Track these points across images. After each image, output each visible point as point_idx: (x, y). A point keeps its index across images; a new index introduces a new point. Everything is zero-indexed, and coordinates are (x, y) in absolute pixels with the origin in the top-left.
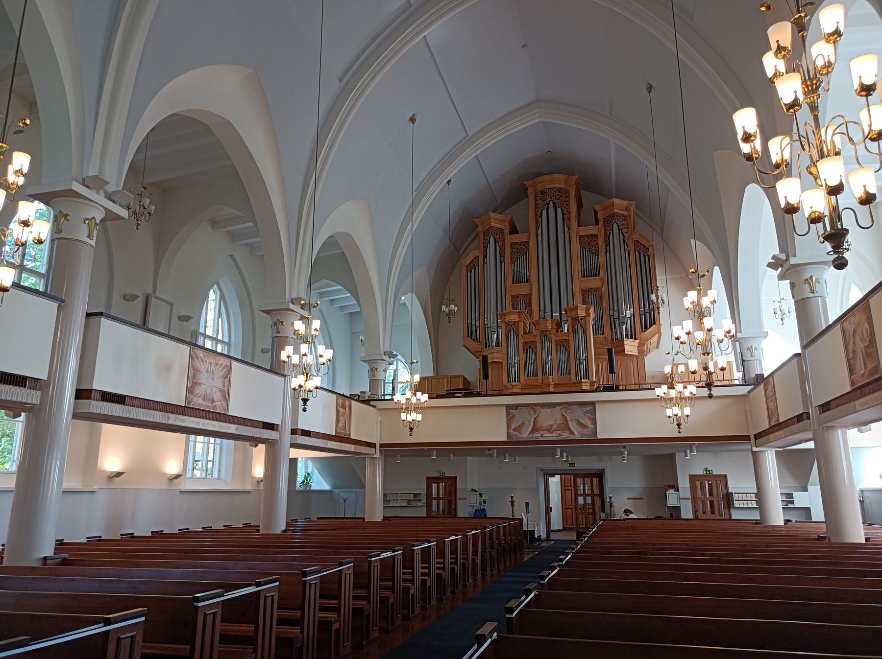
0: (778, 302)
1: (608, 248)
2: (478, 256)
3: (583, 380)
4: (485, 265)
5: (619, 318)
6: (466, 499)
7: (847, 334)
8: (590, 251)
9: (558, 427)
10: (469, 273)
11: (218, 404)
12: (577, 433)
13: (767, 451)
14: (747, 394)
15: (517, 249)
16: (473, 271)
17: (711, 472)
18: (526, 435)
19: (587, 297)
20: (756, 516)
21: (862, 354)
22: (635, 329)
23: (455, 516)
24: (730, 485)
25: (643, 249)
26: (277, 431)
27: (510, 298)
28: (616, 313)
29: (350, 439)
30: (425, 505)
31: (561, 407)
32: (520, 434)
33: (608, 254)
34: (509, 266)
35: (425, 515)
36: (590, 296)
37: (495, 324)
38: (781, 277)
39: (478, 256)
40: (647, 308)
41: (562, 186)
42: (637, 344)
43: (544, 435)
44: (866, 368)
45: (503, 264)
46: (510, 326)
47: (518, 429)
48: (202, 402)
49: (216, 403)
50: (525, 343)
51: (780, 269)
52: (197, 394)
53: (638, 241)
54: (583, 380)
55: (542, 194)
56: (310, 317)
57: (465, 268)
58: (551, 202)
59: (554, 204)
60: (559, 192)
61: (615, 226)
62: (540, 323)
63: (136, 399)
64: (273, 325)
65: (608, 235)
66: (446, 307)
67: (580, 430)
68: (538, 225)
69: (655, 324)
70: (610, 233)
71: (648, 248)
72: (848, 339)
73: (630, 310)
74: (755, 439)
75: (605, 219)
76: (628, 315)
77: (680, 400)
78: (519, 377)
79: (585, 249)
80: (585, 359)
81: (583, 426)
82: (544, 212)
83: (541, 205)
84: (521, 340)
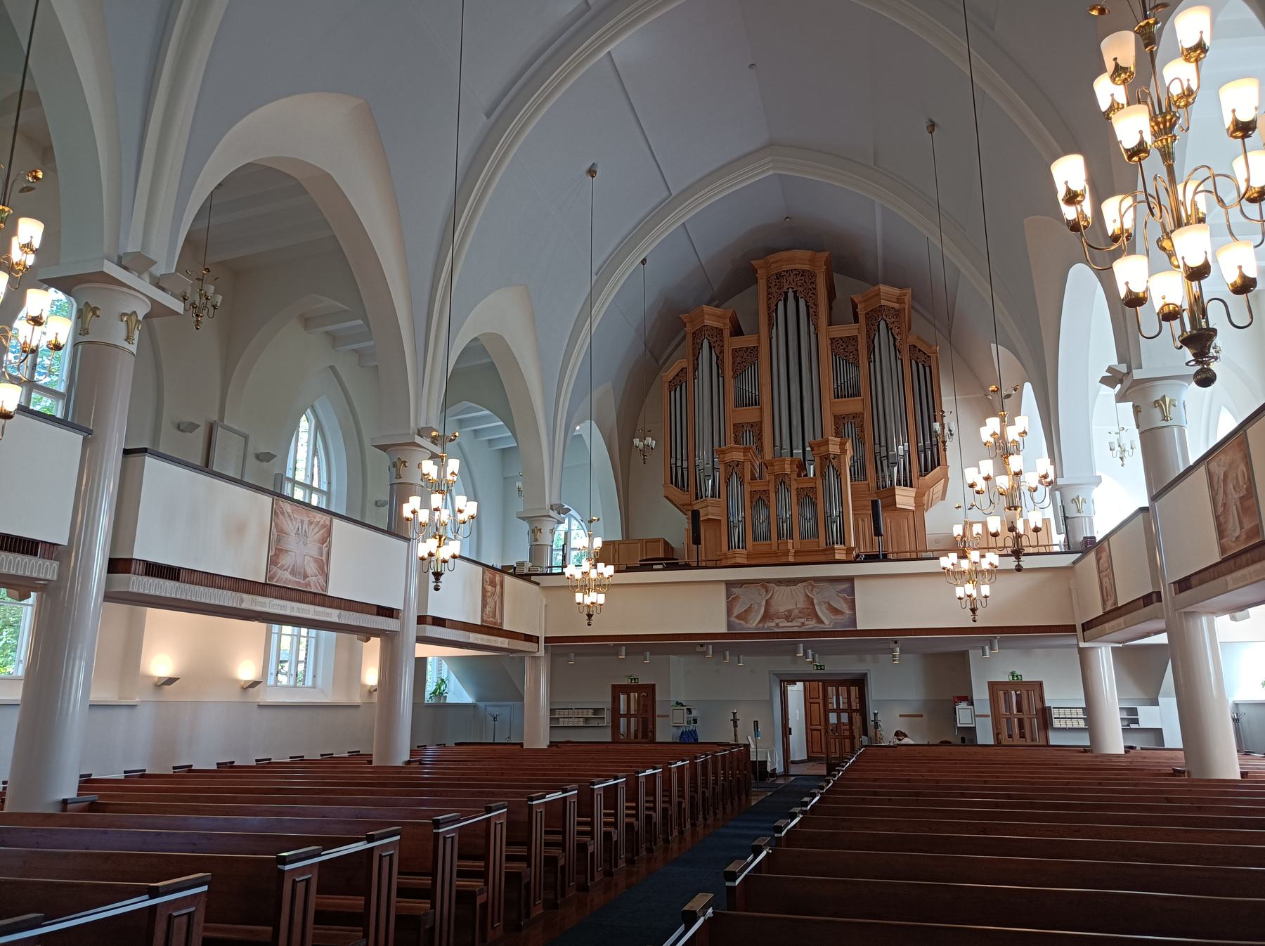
0: (1116, 433)
1: (872, 356)
2: (686, 368)
3: (836, 546)
4: (696, 380)
5: (887, 456)
6: (668, 716)
7: (1215, 479)
8: (846, 360)
9: (800, 612)
10: (673, 393)
11: (312, 580)
12: (828, 622)
13: (1101, 647)
14: (1072, 565)
15: (742, 357)
16: (678, 389)
17: (1019, 677)
18: (754, 625)
19: (842, 426)
20: (1084, 740)
21: (1237, 508)
22: (910, 472)
23: (653, 741)
24: (1047, 696)
25: (923, 357)
26: (397, 618)
27: (732, 428)
28: (883, 450)
29: (502, 629)
30: (610, 724)
31: (805, 584)
32: (747, 622)
33: (872, 364)
34: (730, 382)
35: (610, 740)
36: (846, 425)
37: (710, 465)
38: (1121, 398)
39: (686, 368)
40: (928, 442)
41: (806, 267)
42: (913, 494)
43: (780, 625)
44: (1242, 528)
45: (721, 379)
46: (732, 467)
47: (743, 616)
48: (290, 577)
49: (310, 578)
50: (753, 493)
51: (1119, 386)
52: (282, 566)
53: (915, 347)
54: (836, 546)
55: (778, 278)
56: (444, 455)
57: (667, 385)
58: (790, 290)
59: (795, 292)
60: (802, 275)
61: (882, 324)
62: (775, 464)
63: (196, 573)
64: (391, 467)
65: (872, 337)
66: (640, 441)
67: (833, 617)
68: (771, 323)
69: (939, 464)
70: (875, 334)
71: (929, 357)
72: (1216, 487)
73: (903, 445)
74: (1084, 631)
75: (868, 314)
76: (901, 453)
77: (976, 575)
78: (744, 541)
79: (839, 357)
80: (839, 516)
81: (836, 611)
82: (781, 304)
83: (776, 295)
84: (748, 488)
